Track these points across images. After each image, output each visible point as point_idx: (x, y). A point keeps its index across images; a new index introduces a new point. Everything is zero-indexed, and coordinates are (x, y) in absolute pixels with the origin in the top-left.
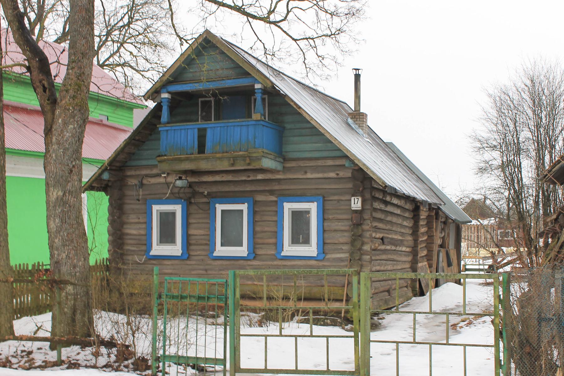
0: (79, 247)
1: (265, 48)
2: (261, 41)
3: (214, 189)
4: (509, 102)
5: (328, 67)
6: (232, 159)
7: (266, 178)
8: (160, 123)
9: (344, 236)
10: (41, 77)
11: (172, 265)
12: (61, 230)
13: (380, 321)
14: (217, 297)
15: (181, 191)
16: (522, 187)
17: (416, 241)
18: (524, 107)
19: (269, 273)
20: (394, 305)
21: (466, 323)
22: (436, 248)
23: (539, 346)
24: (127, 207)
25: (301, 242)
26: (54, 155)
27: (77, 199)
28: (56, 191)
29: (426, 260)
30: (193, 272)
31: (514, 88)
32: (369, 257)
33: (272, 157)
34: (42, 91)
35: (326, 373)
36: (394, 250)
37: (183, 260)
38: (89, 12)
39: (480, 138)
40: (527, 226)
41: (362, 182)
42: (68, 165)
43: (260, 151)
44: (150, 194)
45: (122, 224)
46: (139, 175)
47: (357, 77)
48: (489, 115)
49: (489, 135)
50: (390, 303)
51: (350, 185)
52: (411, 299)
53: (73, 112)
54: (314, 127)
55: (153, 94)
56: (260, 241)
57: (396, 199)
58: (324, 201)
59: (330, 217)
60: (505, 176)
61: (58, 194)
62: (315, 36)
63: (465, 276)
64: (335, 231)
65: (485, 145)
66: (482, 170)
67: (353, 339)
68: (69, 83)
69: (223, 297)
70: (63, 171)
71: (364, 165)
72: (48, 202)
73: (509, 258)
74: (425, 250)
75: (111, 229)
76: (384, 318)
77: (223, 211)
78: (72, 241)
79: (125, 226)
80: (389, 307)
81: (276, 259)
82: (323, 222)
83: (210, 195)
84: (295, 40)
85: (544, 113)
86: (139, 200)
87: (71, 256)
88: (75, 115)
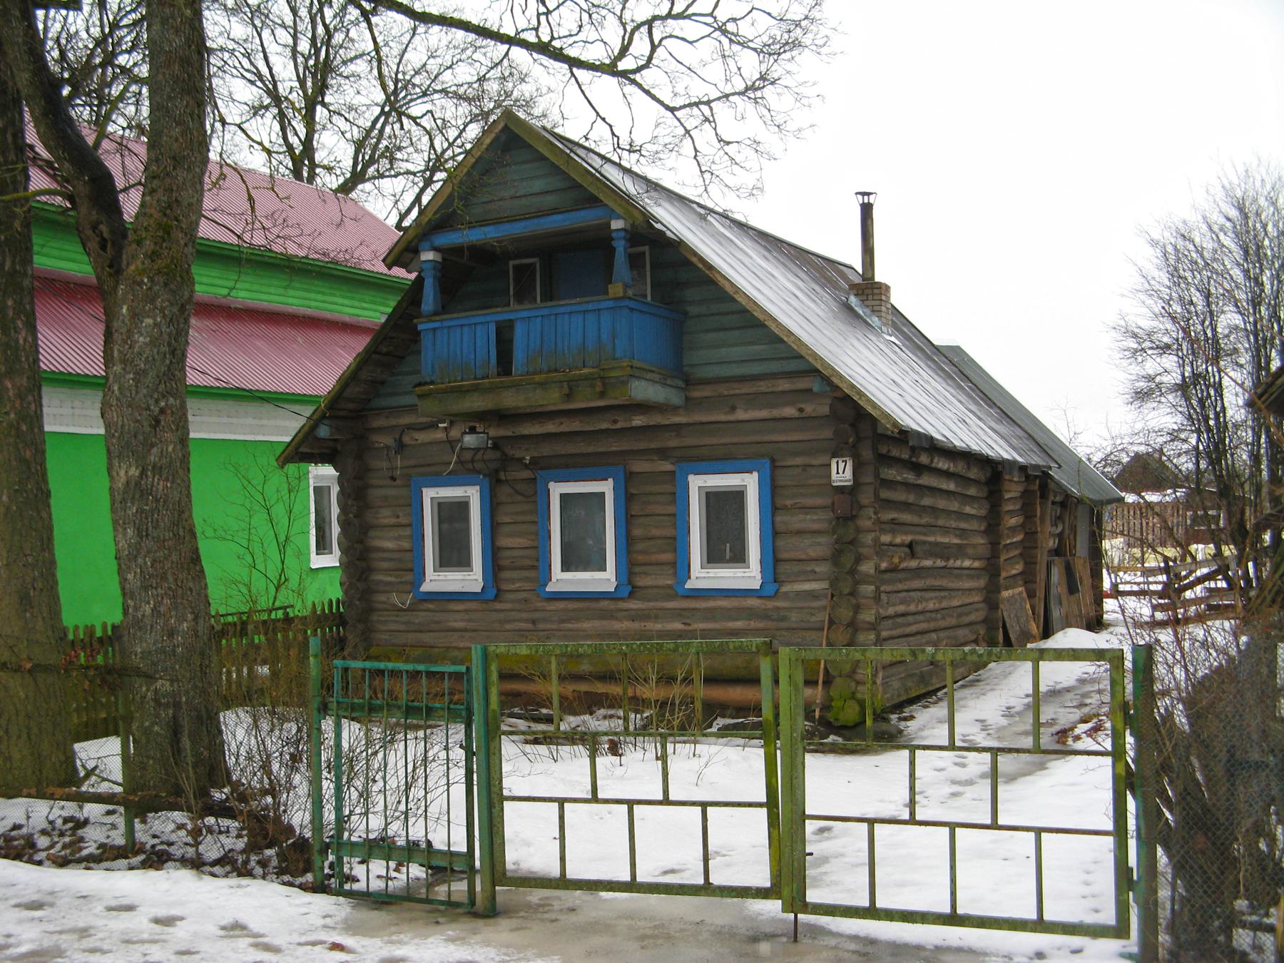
0: (180, 591)
1: (613, 134)
2: (604, 119)
3: (546, 450)
4: (1194, 255)
5: (742, 165)
6: (565, 385)
7: (651, 423)
8: (419, 315)
9: (819, 544)
10: (94, 215)
11: (466, 611)
12: (138, 551)
13: (902, 725)
14: (449, 708)
15: (477, 457)
16: (1222, 427)
17: (995, 545)
18: (1226, 263)
19: (564, 650)
20: (943, 684)
21: (1089, 725)
22: (1042, 558)
23: (1231, 834)
24: (374, 494)
25: (728, 557)
26: (116, 388)
27: (173, 483)
28: (124, 466)
29: (1020, 582)
30: (508, 627)
31: (1205, 227)
32: (873, 587)
33: (656, 377)
34: (97, 246)
35: (703, 892)
36: (944, 568)
37: (487, 601)
38: (189, 64)
39: (1136, 330)
40: (266, 817)
41: (852, 425)
42: (148, 409)
43: (625, 364)
44: (415, 466)
45: (366, 529)
46: (396, 426)
47: (867, 210)
48: (1152, 282)
49: (1155, 324)
50: (934, 681)
51: (827, 433)
52: (985, 665)
53: (150, 289)
54: (744, 311)
55: (403, 253)
56: (641, 558)
57: (943, 459)
58: (774, 467)
59: (789, 503)
60: (1190, 406)
61: (130, 473)
62: (714, 94)
63: (1036, 655)
64: (800, 532)
65: (1147, 344)
66: (1142, 396)
67: (764, 810)
68: (145, 224)
69: (462, 707)
70: (137, 421)
71: (853, 386)
72: (111, 489)
73: (1205, 571)
74: (1018, 563)
75: (344, 540)
76: (912, 718)
77: (564, 497)
78: (164, 577)
79: (372, 533)
80: (931, 688)
81: (675, 596)
82: (773, 515)
83: (536, 464)
84: (672, 110)
85: (1268, 273)
86: (393, 479)
87: (162, 609)
88: (156, 296)
